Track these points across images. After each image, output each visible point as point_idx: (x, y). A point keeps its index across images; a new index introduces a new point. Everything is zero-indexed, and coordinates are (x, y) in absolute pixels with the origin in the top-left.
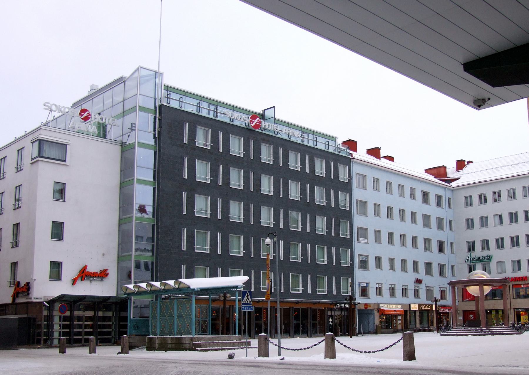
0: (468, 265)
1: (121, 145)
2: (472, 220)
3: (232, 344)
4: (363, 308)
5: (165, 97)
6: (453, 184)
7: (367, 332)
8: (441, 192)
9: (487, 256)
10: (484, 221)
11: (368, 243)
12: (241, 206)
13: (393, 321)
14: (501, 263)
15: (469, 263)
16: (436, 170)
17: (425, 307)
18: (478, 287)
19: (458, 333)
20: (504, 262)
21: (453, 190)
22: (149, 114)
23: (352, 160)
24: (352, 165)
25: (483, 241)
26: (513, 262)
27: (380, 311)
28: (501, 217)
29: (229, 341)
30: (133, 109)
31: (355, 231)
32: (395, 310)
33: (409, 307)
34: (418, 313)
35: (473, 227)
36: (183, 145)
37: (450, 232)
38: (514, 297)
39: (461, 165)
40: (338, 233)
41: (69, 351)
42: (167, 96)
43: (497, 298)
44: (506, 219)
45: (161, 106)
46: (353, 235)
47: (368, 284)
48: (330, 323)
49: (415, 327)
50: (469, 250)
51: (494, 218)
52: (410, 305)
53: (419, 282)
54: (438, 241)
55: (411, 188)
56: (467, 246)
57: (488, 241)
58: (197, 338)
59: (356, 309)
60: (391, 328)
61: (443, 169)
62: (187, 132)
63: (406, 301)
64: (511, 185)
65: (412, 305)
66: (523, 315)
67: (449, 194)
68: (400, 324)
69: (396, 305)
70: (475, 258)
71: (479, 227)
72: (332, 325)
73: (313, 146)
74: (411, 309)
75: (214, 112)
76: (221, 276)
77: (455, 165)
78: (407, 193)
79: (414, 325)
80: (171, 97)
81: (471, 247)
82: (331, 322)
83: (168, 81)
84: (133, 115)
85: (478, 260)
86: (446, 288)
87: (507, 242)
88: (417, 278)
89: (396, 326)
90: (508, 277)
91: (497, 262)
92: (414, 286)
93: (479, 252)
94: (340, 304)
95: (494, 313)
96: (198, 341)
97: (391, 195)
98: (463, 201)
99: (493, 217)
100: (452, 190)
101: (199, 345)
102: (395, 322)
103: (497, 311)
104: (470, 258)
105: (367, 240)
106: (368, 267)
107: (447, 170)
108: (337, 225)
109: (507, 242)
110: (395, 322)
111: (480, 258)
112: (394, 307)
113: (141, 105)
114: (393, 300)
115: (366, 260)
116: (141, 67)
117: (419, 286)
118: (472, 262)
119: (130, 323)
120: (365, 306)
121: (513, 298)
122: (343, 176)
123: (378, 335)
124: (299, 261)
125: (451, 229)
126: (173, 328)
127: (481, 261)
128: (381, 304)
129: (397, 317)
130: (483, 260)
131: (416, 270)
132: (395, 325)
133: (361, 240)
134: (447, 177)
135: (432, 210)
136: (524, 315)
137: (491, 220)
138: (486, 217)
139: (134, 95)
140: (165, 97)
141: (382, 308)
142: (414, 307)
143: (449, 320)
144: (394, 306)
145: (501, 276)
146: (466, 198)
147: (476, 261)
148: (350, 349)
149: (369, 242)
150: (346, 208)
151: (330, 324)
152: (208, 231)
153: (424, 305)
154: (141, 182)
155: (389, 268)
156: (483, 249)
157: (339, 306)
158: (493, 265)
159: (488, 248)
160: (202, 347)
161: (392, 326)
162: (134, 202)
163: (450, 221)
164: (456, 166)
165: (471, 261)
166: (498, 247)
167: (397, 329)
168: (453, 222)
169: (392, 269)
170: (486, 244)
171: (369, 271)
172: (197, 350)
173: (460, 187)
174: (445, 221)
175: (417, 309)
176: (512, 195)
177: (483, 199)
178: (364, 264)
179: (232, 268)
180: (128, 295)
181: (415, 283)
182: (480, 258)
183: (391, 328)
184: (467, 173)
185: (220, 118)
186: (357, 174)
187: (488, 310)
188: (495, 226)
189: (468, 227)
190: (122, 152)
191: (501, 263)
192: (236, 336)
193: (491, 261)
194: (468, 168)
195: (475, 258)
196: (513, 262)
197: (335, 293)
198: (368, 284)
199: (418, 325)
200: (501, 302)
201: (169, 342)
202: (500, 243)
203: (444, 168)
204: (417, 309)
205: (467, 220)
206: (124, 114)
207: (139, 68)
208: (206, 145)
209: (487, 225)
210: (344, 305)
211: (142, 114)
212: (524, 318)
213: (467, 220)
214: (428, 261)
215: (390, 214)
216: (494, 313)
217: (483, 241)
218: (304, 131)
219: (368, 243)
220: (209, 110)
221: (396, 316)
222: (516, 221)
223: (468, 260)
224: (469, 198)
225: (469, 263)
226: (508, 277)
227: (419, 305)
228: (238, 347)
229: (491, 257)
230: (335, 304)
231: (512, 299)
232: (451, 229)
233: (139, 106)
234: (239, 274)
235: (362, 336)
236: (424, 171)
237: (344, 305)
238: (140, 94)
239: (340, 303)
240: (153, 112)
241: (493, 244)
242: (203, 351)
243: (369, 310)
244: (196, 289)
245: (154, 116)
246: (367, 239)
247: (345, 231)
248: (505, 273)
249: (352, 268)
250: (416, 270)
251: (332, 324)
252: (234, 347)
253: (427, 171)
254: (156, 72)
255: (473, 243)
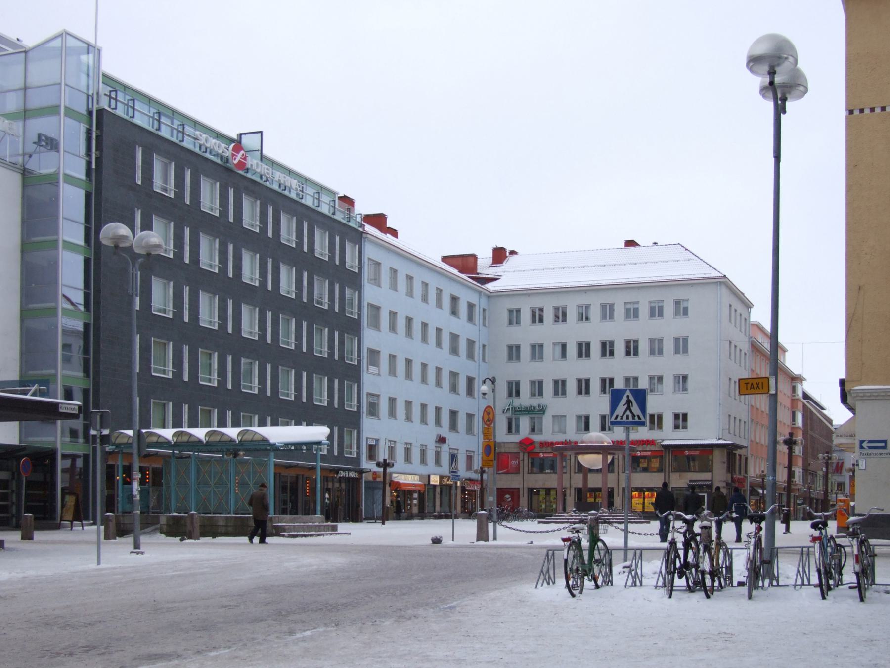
0: (506, 417)
1: (22, 172)
2: (518, 347)
3: (322, 527)
4: (370, 478)
5: (105, 95)
6: (491, 286)
7: (370, 516)
8: (474, 299)
9: (539, 406)
10: (537, 350)
11: (379, 374)
12: (214, 303)
13: (407, 501)
14: (560, 419)
15: (509, 414)
16: (460, 259)
17: (448, 480)
18: (600, 456)
19: (570, 520)
20: (565, 416)
21: (490, 296)
22: (81, 124)
23: (364, 235)
24: (364, 245)
25: (533, 383)
26: (579, 417)
27: (392, 485)
28: (564, 346)
29: (311, 524)
30: (53, 110)
31: (365, 354)
32: (414, 484)
33: (427, 480)
34: (438, 490)
35: (518, 358)
36: (133, 187)
37: (482, 364)
38: (576, 471)
39: (499, 255)
40: (342, 357)
41: (38, 535)
42: (109, 94)
43: (547, 471)
44: (572, 350)
45: (101, 112)
46: (362, 362)
47: (377, 440)
48: (327, 501)
49: (449, 511)
50: (510, 395)
51: (554, 349)
52: (429, 476)
53: (442, 440)
54: (467, 376)
55: (437, 289)
56: (474, 385)
57: (541, 383)
58: (277, 519)
59: (362, 481)
60: (404, 511)
61: (472, 259)
62: (140, 164)
63: (424, 470)
64: (583, 300)
65: (432, 477)
66: (648, 497)
67: (484, 302)
68: (415, 505)
69: (413, 476)
70: (519, 408)
71: (529, 361)
72: (330, 504)
73: (313, 207)
74: (432, 483)
75: (179, 131)
76: (257, 425)
77: (490, 254)
78: (418, 290)
79: (432, 509)
80: (118, 99)
81: (514, 389)
82: (328, 499)
83: (110, 67)
84: (53, 119)
85: (524, 411)
86: (474, 452)
87: (571, 387)
88: (440, 435)
89: (410, 508)
90: (569, 440)
91: (553, 417)
92: (436, 447)
93: (525, 399)
94: (344, 471)
95: (543, 493)
96: (279, 522)
97: (411, 299)
98: (505, 315)
99: (552, 346)
100: (489, 297)
101: (283, 528)
102: (409, 502)
103: (548, 491)
104: (511, 407)
105: (379, 370)
106: (378, 413)
107: (479, 261)
108: (342, 343)
109: (571, 387)
110: (409, 502)
111: (527, 408)
112: (410, 479)
113: (67, 105)
114: (408, 468)
115: (376, 402)
116: (68, 33)
117: (440, 448)
118: (515, 414)
119: (123, 492)
120: (374, 476)
121: (575, 473)
122: (351, 262)
123: (425, 521)
124: (291, 398)
125: (484, 360)
126: (227, 503)
127: (529, 412)
128: (394, 473)
129: (413, 495)
130: (532, 411)
131: (438, 422)
132: (409, 507)
133: (372, 369)
134: (478, 274)
135: (461, 326)
136: (637, 498)
137: (548, 351)
138: (541, 346)
139: (52, 83)
140: (105, 95)
141: (396, 480)
142: (435, 480)
143: (475, 502)
144: (410, 477)
145: (560, 438)
146: (510, 311)
147: (521, 413)
148: (561, 529)
149: (381, 373)
150: (352, 315)
151: (327, 503)
152: (169, 340)
153: (446, 477)
154: (69, 246)
155: (404, 417)
156: (533, 395)
157: (342, 474)
158: (547, 421)
159: (541, 394)
160: (287, 531)
161: (406, 508)
162: (60, 283)
163: (484, 346)
164: (492, 256)
165: (512, 412)
166: (556, 393)
167: (412, 513)
168: (486, 348)
169: (408, 419)
170: (538, 388)
171: (380, 419)
172: (283, 536)
173: (499, 293)
174: (477, 345)
175: (438, 483)
176: (584, 317)
177: (537, 317)
178: (373, 411)
179: (246, 413)
180: (117, 447)
181: (436, 441)
182: (527, 408)
183: (404, 511)
184: (512, 270)
185: (188, 144)
186: (369, 259)
187: (645, 488)
188: (554, 359)
189: (510, 358)
190: (25, 186)
191: (560, 419)
192: (316, 516)
193: (544, 413)
194: (510, 263)
195: (519, 408)
196: (579, 417)
197: (336, 454)
198: (377, 440)
199: (438, 508)
200: (555, 477)
201: (221, 523)
202: (560, 387)
203: (474, 257)
204: (438, 483)
205: (510, 347)
206: (26, 114)
207: (64, 35)
208: (166, 190)
209: (541, 358)
210: (349, 473)
211: (70, 121)
212: (638, 502)
213: (510, 347)
214: (454, 409)
215: (393, 327)
216: (543, 493)
217: (533, 383)
218: (305, 181)
219: (379, 374)
220: (172, 128)
221: (411, 493)
222: (588, 355)
223: (508, 409)
224: (515, 312)
225: (509, 414)
226: (569, 440)
227: (441, 477)
228: (330, 532)
229: (545, 408)
230: (337, 471)
231: (572, 474)
232: (484, 360)
233: (66, 107)
234: (251, 422)
235: (376, 522)
236: (441, 259)
237: (349, 473)
238: (66, 85)
239: (344, 470)
240: (85, 119)
241: (548, 388)
242: (291, 538)
243: (378, 482)
244: (277, 444)
245: (87, 126)
246: (378, 366)
247: (350, 353)
248: (565, 433)
249: (358, 414)
250: (438, 422)
251: (328, 502)
252: (320, 531)
253: (445, 259)
254: (89, 45)
255: (518, 383)
